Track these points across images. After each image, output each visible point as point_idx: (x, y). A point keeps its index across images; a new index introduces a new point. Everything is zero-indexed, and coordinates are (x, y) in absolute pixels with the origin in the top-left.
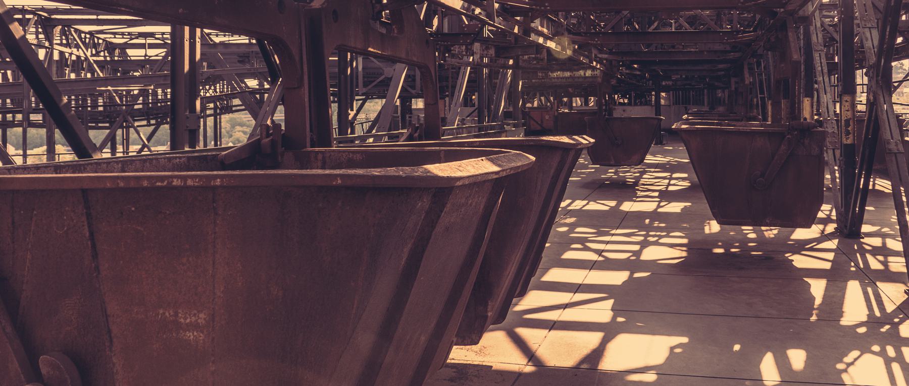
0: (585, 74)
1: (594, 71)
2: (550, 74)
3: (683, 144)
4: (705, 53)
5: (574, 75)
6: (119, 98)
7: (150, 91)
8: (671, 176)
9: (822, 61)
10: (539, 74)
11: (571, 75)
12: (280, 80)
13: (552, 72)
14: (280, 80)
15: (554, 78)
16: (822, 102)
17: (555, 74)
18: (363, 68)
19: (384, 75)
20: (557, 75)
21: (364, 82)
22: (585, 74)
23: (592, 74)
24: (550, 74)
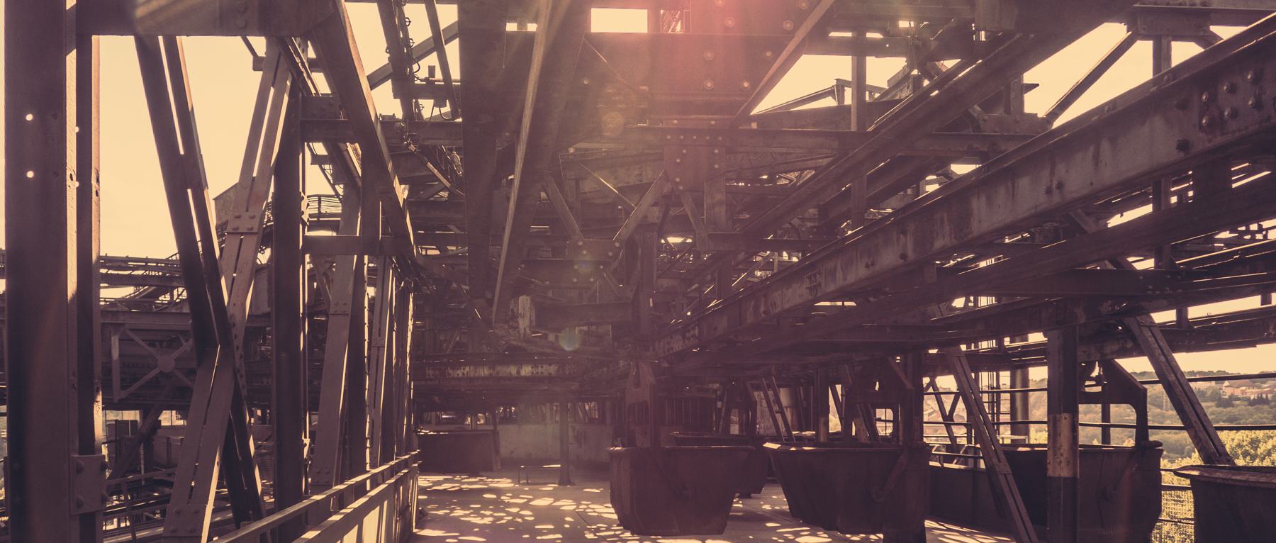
0: (518, 372)
1: (537, 367)
2: (450, 371)
3: (780, 490)
4: (888, 330)
5: (498, 373)
6: (771, 442)
7: (371, 265)
8: (514, 518)
9: (1161, 344)
10: (427, 371)
11: (491, 374)
12: (847, 304)
13: (453, 369)
14: (847, 304)
15: (459, 379)
16: (1068, 420)
17: (459, 372)
18: (120, 355)
19: (156, 367)
20: (463, 374)
21: (122, 380)
22: (518, 372)
23: (533, 373)
24: (450, 371)
